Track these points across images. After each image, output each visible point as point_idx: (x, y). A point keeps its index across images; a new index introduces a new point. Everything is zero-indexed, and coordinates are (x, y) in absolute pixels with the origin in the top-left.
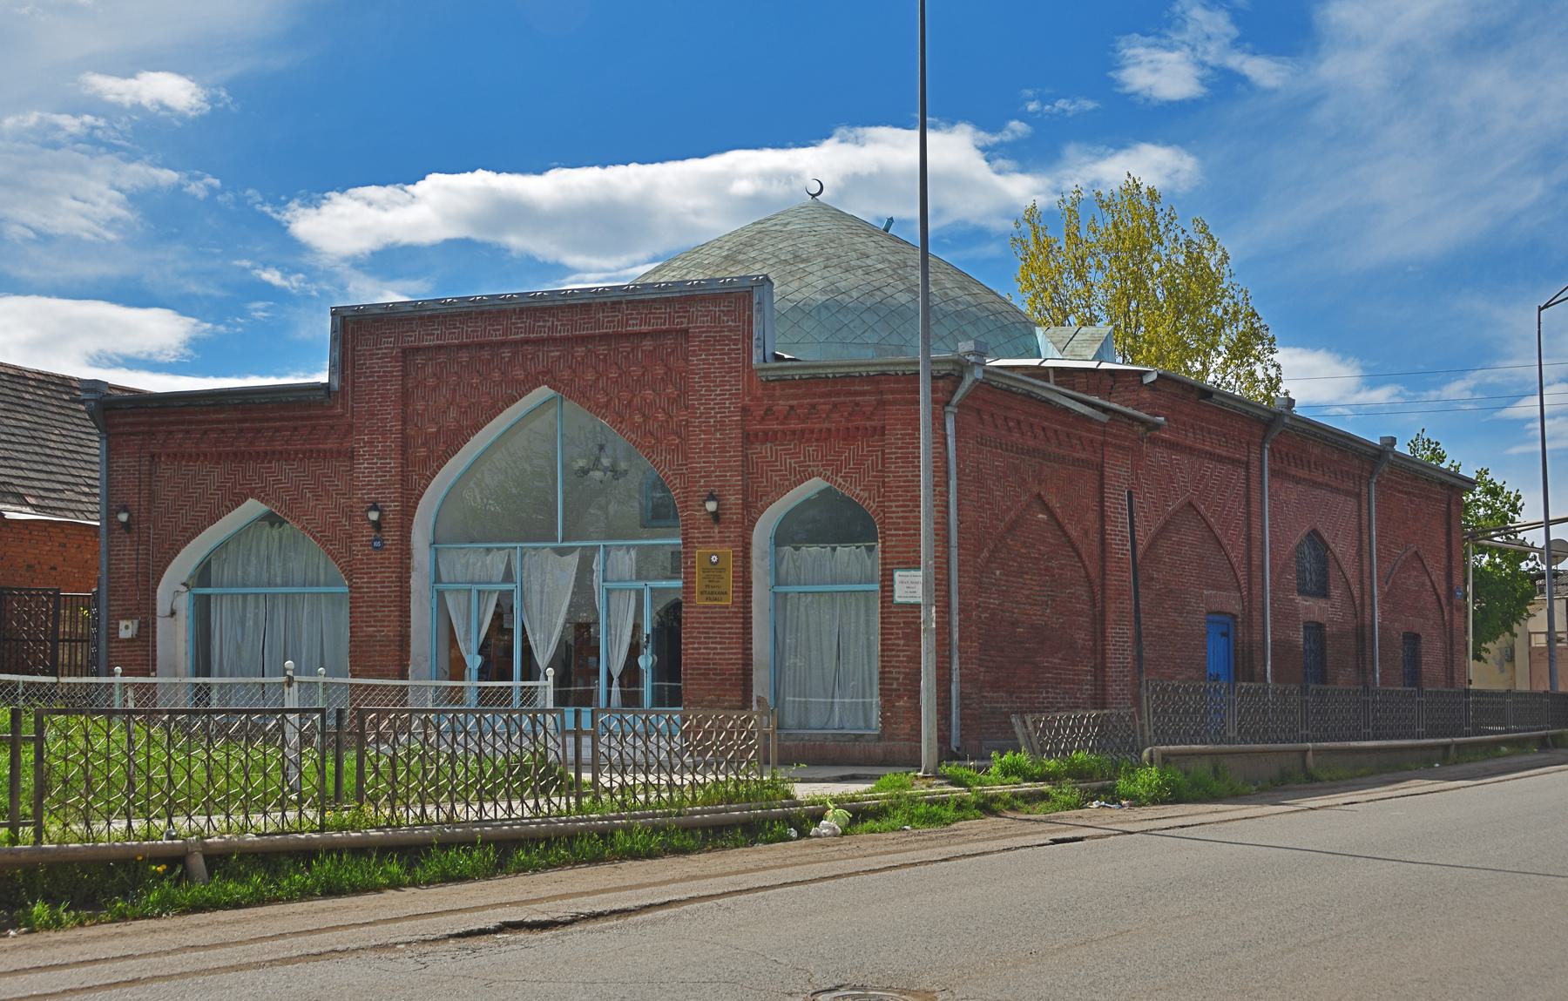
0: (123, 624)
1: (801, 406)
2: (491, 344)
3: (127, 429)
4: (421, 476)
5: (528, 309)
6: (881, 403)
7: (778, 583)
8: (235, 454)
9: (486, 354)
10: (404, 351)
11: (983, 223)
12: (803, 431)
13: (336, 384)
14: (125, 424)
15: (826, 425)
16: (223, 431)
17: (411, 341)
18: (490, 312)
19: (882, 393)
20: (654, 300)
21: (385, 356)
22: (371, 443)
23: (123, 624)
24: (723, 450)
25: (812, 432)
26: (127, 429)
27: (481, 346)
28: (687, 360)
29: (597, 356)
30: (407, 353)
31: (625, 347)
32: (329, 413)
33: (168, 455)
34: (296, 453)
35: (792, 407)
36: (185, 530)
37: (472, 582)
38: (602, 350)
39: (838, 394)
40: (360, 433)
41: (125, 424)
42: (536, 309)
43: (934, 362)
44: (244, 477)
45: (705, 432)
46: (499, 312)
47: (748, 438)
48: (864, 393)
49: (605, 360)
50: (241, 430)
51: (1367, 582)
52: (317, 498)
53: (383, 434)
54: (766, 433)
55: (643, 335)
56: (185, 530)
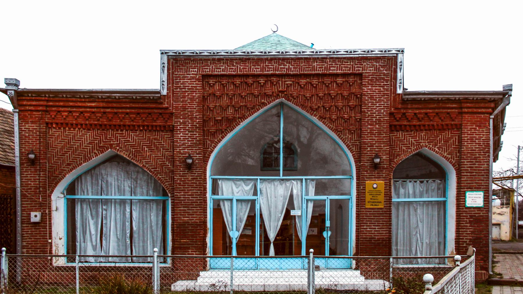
0: (33, 214)
1: (420, 113)
2: (254, 76)
3: (32, 108)
4: (212, 142)
5: (275, 59)
6: (461, 113)
7: (351, 268)
8: (101, 125)
9: (250, 81)
10: (203, 76)
11: (249, 50)
12: (419, 126)
13: (165, 92)
14: (30, 105)
15: (432, 123)
16: (93, 112)
17: (207, 71)
18: (253, 59)
19: (461, 108)
20: (345, 58)
21: (193, 78)
22: (184, 123)
23: (33, 214)
24: (380, 134)
25: (424, 126)
26: (32, 108)
27: (247, 76)
28: (361, 88)
29: (312, 85)
30: (205, 77)
31: (327, 80)
32: (160, 106)
33: (57, 124)
34: (139, 126)
35: (415, 114)
36: (69, 164)
37: (283, 180)
38: (315, 81)
39: (439, 108)
40: (177, 117)
41: (30, 105)
42: (279, 59)
43: (260, 254)
44: (106, 138)
45: (371, 125)
46: (258, 59)
47: (393, 128)
48: (452, 108)
49: (316, 87)
50: (105, 113)
51: (145, 231)
52: (152, 151)
53: (191, 119)
54: (400, 126)
55: (337, 75)
56: (69, 164)
